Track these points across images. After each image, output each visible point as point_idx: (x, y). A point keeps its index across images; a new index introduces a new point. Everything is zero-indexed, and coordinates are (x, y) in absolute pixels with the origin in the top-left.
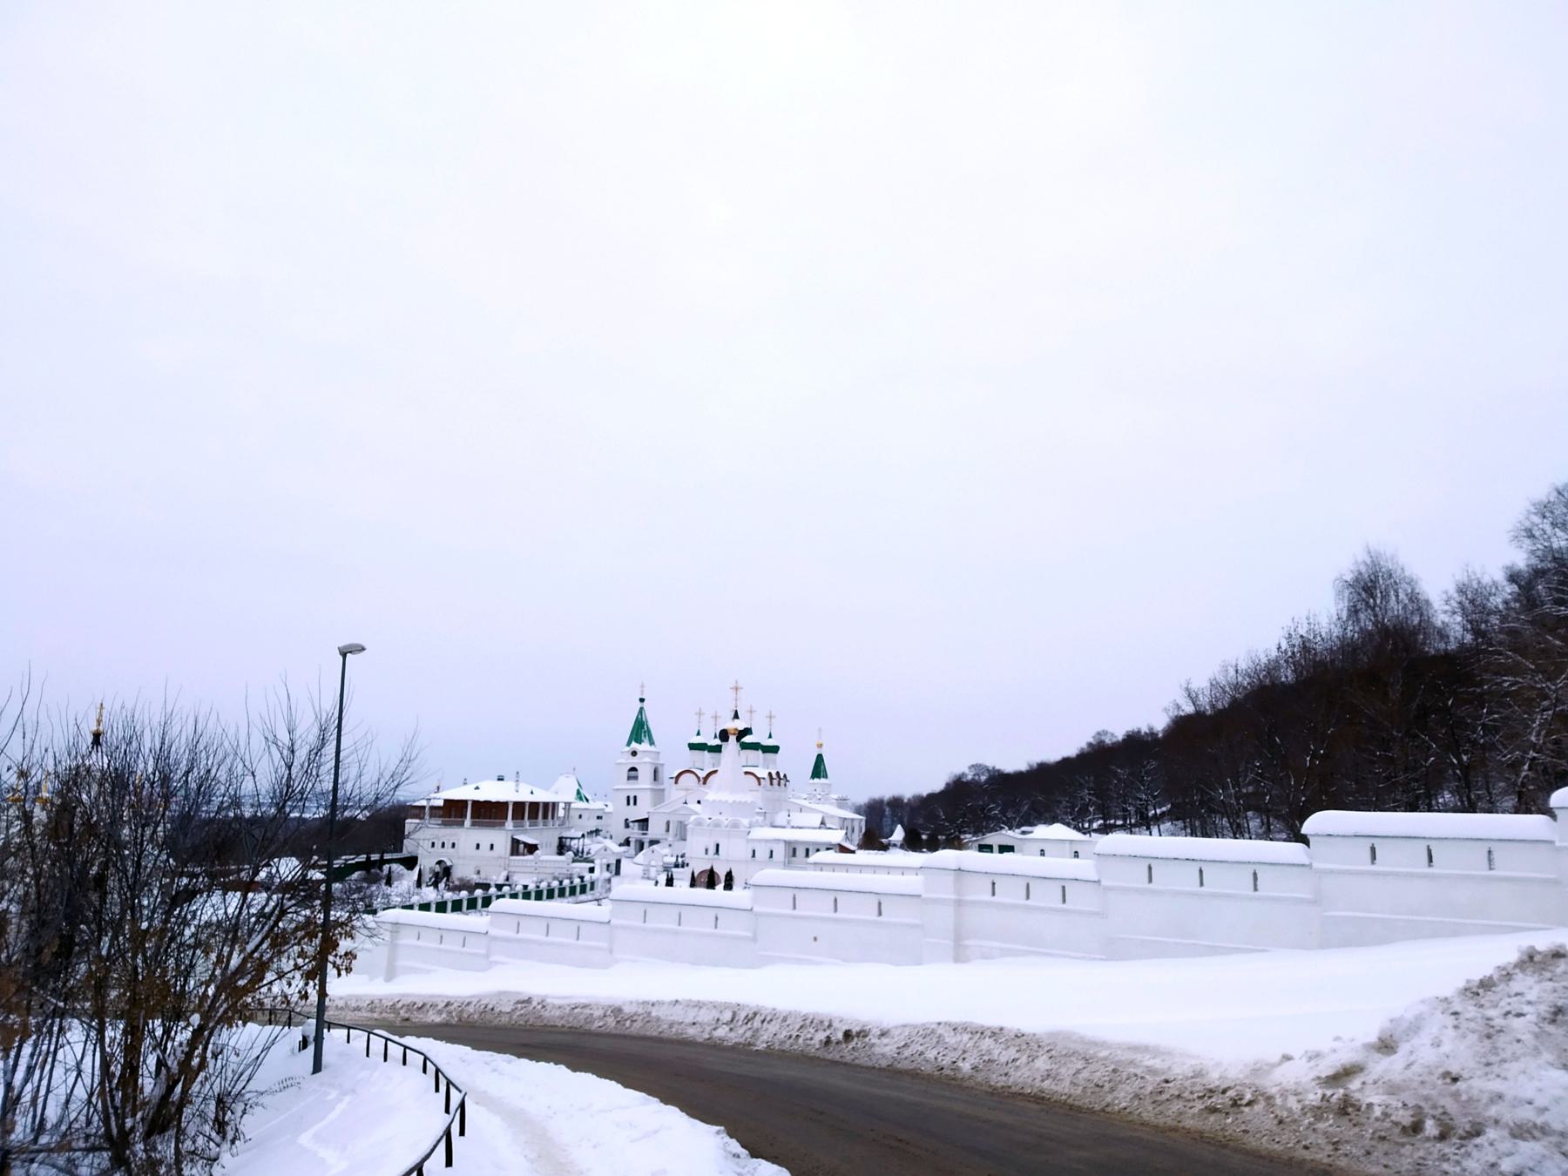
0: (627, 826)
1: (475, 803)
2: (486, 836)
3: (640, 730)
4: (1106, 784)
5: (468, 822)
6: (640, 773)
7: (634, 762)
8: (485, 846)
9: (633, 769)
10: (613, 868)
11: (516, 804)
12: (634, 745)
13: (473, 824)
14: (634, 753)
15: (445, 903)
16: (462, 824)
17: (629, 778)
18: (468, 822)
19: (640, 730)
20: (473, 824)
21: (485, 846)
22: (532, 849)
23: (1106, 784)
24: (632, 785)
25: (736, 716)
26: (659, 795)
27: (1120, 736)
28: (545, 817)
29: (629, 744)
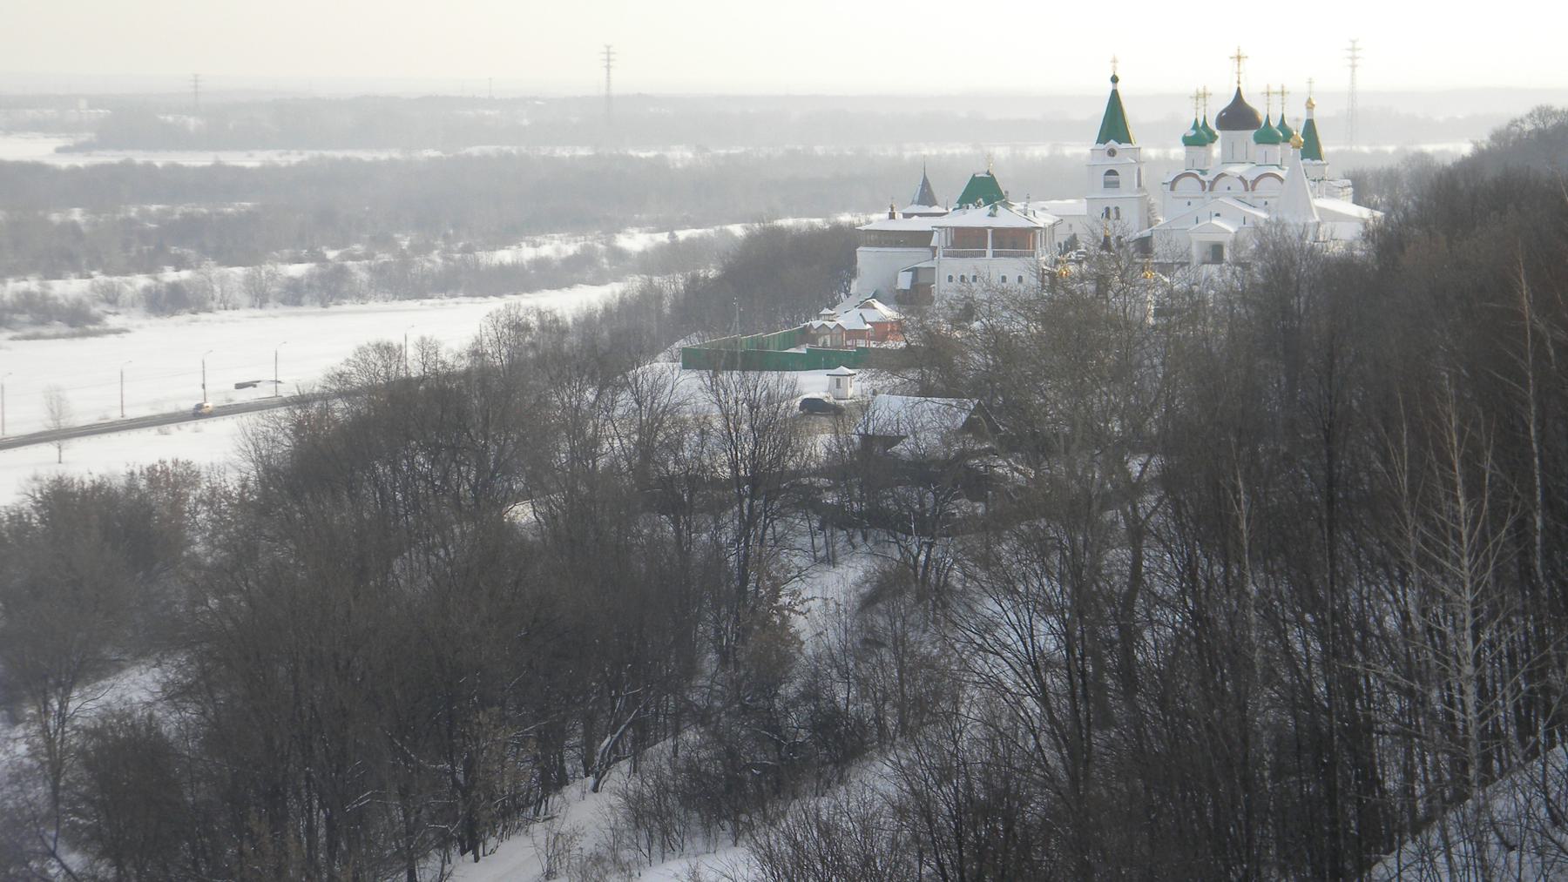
1: (996, 231)
5: (989, 252)
12: (1112, 143)
17: (1107, 185)
18: (989, 252)
24: (1111, 193)
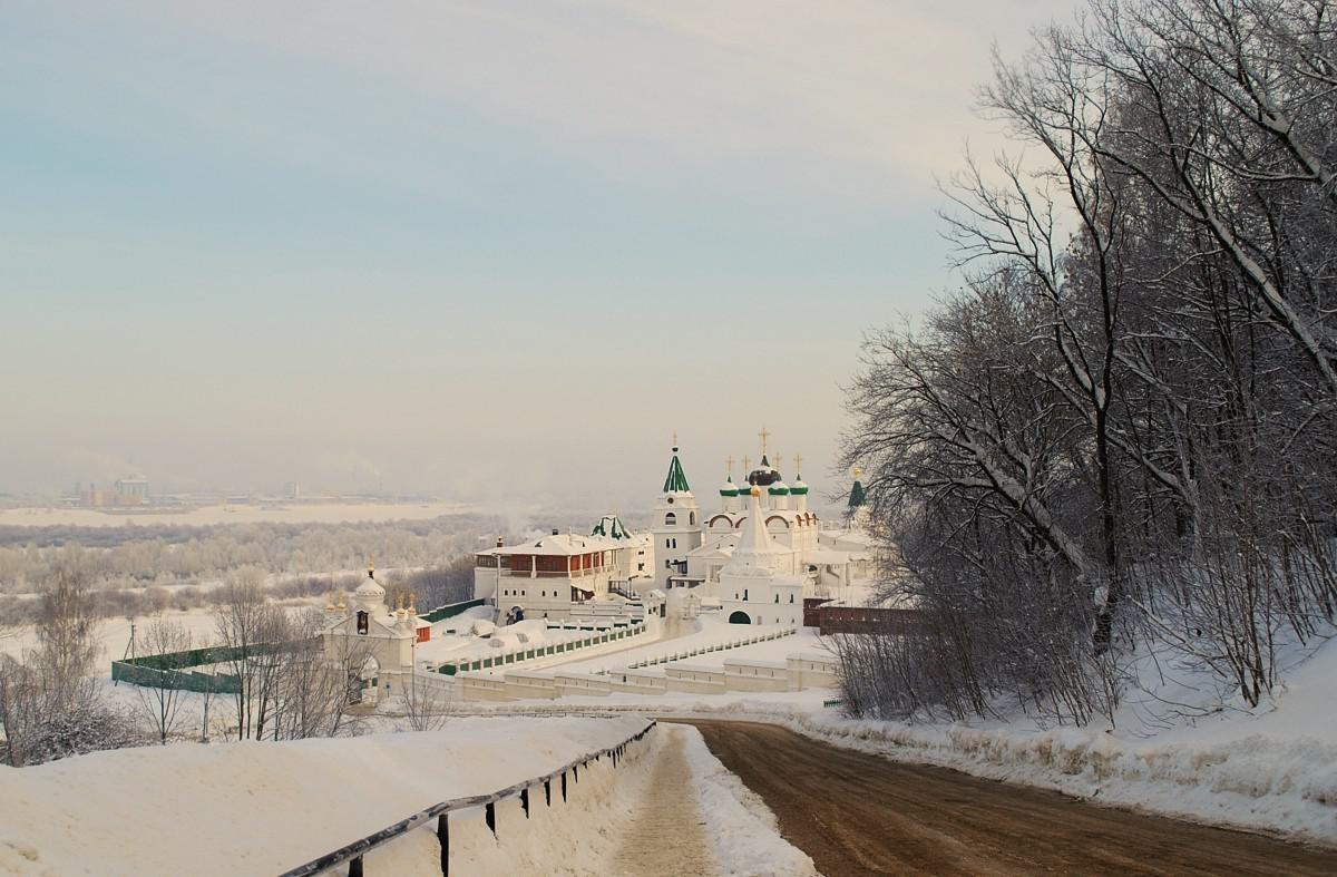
0: (668, 567)
2: (549, 584)
3: (677, 480)
4: (527, 811)
5: (534, 573)
6: (677, 519)
7: (670, 508)
8: (549, 594)
9: (671, 515)
10: (659, 610)
11: (584, 555)
12: (672, 493)
13: (538, 576)
14: (671, 501)
15: (598, 639)
16: (567, 575)
17: (667, 523)
18: (534, 573)
19: (677, 480)
20: (538, 576)
21: (549, 594)
22: (589, 595)
23: (527, 811)
24: (671, 529)
25: (765, 462)
26: (695, 542)
27: (773, 815)
28: (596, 565)
29: (666, 490)
